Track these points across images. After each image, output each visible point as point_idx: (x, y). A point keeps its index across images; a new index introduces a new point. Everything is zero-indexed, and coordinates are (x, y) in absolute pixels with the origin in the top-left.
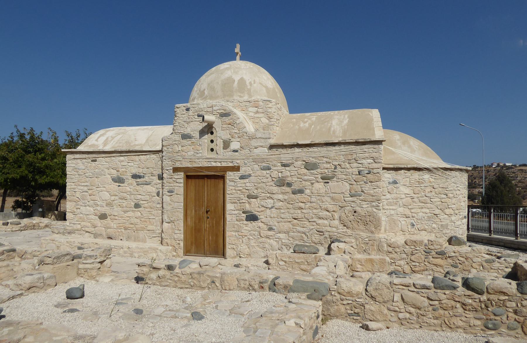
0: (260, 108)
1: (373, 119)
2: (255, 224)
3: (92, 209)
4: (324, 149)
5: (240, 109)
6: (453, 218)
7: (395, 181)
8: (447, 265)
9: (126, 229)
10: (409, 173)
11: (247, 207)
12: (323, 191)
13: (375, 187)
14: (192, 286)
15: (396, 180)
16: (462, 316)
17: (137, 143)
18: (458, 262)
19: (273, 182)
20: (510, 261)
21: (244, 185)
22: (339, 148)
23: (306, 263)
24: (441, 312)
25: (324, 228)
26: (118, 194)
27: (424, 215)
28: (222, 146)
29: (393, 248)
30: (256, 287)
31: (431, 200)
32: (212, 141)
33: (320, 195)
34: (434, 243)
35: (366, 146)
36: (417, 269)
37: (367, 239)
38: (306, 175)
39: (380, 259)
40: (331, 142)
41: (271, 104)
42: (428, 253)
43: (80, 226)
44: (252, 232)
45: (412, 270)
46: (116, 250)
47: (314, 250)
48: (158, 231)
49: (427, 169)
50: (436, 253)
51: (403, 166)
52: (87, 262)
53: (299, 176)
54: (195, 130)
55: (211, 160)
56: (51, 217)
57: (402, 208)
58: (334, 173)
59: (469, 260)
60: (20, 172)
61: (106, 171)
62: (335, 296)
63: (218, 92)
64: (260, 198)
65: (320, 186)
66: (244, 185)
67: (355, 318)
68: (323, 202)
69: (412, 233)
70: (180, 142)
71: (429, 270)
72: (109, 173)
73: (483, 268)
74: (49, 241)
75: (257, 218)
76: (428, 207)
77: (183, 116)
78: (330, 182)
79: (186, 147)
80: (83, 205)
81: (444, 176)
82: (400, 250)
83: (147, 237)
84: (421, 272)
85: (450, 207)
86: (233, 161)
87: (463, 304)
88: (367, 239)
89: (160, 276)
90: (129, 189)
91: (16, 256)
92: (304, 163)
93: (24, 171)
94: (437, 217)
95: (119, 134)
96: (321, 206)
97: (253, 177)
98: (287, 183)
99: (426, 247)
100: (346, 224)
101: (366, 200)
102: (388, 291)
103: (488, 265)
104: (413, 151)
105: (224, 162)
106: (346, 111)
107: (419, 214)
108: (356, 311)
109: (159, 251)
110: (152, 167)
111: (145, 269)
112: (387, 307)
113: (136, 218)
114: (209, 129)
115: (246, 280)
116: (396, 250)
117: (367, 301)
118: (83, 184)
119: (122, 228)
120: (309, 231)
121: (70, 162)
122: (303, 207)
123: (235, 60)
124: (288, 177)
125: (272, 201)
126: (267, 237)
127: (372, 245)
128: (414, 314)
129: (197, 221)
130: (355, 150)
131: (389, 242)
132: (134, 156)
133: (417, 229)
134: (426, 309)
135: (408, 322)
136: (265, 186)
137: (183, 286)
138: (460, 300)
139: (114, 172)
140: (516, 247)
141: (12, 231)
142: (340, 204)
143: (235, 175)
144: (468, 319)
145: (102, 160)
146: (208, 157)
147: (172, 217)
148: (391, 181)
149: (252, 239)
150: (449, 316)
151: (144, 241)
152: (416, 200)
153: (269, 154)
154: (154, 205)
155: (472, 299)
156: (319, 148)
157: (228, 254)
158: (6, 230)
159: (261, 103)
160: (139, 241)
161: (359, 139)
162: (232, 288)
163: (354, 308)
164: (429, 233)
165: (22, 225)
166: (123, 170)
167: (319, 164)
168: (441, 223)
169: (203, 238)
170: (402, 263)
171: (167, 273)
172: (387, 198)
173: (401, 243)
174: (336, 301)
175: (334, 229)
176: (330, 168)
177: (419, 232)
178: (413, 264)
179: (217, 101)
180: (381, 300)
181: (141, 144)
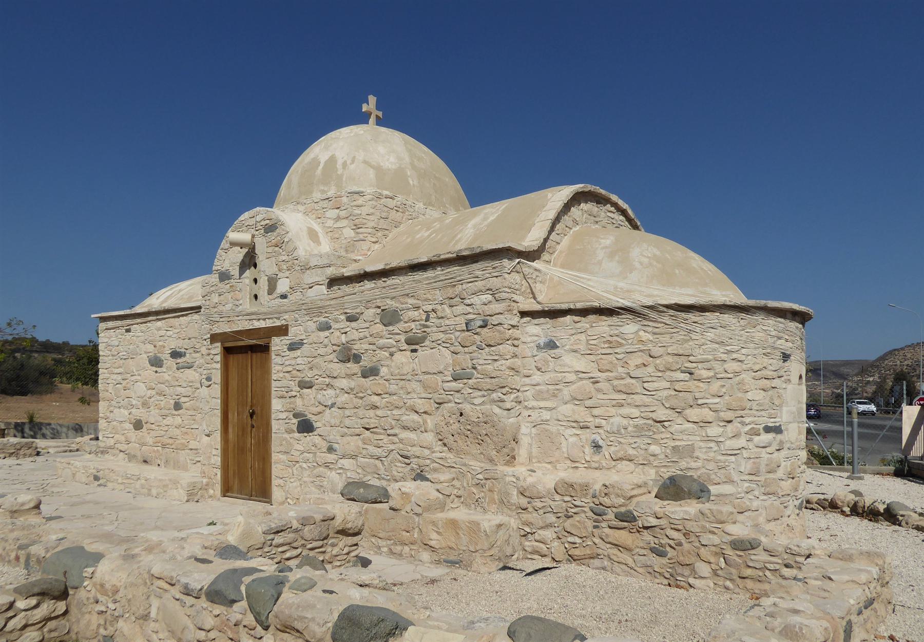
0: (343, 208)
3: (126, 412)
5: (314, 216)
6: (714, 431)
9: (164, 446)
10: (584, 323)
11: (299, 405)
13: (496, 358)
15: (553, 338)
18: (667, 541)
20: (796, 548)
25: (410, 448)
26: (154, 386)
27: (625, 422)
29: (529, 500)
31: (646, 385)
33: (404, 377)
37: (480, 476)
38: (381, 337)
39: (469, 523)
41: (362, 199)
42: (600, 515)
55: (254, 317)
58: (425, 329)
59: (693, 538)
65: (402, 358)
66: (293, 362)
69: (594, 465)
71: (602, 557)
75: (312, 426)
76: (637, 404)
81: (682, 325)
83: (189, 461)
84: (587, 560)
85: (700, 402)
88: (480, 476)
92: (379, 311)
96: (405, 401)
99: (594, 499)
100: (445, 441)
101: (480, 388)
105: (269, 319)
107: (612, 420)
116: (534, 504)
119: (160, 444)
120: (387, 454)
124: (355, 342)
126: (327, 465)
127: (490, 491)
130: (460, 275)
131: (521, 483)
139: (150, 348)
148: (542, 341)
153: (332, 296)
156: (401, 278)
164: (641, 466)
168: (673, 444)
170: (548, 534)
172: (534, 382)
177: (614, 463)
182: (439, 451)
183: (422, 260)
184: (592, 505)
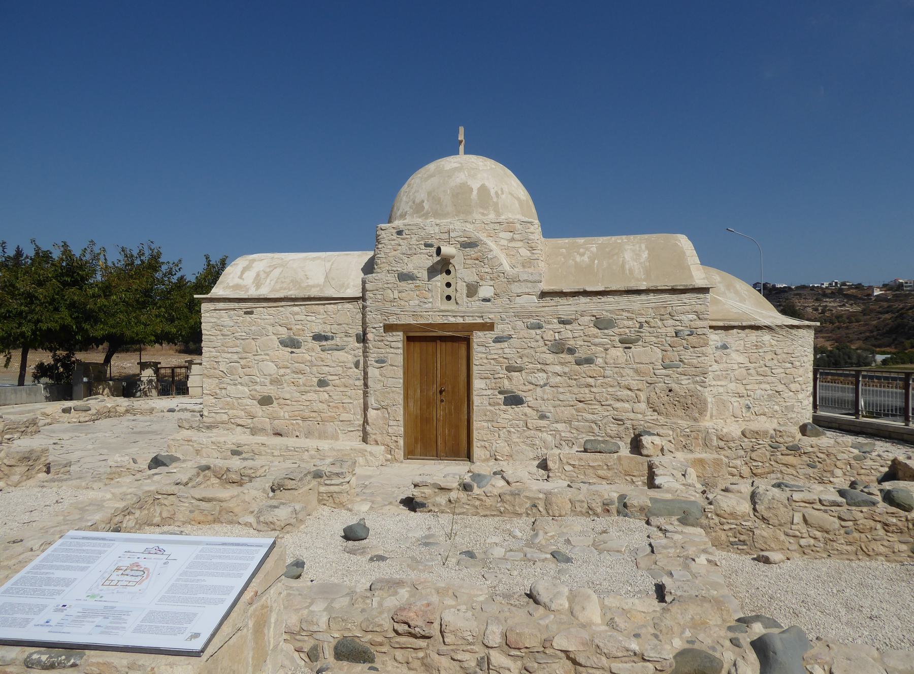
0: (516, 232)
1: (685, 253)
2: (518, 409)
3: (246, 389)
4: (624, 299)
7: (724, 344)
8: (802, 464)
9: (304, 419)
10: (743, 334)
11: (507, 384)
12: (622, 360)
13: (700, 355)
14: (501, 512)
16: (883, 539)
17: (311, 282)
18: (816, 459)
19: (547, 347)
21: (500, 352)
22: (646, 298)
23: (605, 467)
24: (856, 535)
25: (624, 414)
27: (763, 392)
28: (465, 292)
30: (599, 510)
31: (773, 370)
32: (448, 285)
33: (618, 366)
34: (784, 433)
35: (687, 295)
36: (759, 471)
37: (687, 430)
38: (597, 337)
40: (635, 288)
41: (532, 227)
43: (226, 416)
44: (514, 422)
45: (753, 473)
46: (296, 453)
47: (613, 449)
48: (357, 422)
49: (769, 328)
50: (787, 448)
51: (736, 324)
52: (333, 482)
53: (586, 338)
54: (420, 267)
56: (103, 392)
57: (734, 384)
58: (639, 334)
59: (832, 457)
60: (59, 318)
61: (269, 329)
62: (713, 519)
63: (446, 206)
64: (526, 371)
65: (617, 353)
66: (500, 352)
67: (740, 547)
68: (622, 376)
69: (746, 419)
70: (395, 286)
72: (274, 332)
73: (850, 468)
74: (182, 442)
75: (523, 400)
77: (393, 242)
78: (633, 347)
79: (407, 292)
80: (232, 382)
82: (735, 445)
86: (483, 314)
87: (885, 525)
88: (687, 430)
89: (452, 499)
90: (309, 358)
91: (212, 476)
93: (65, 316)
94: (780, 394)
95: (275, 268)
96: (620, 382)
97: (514, 339)
98: (569, 348)
100: (657, 408)
102: (785, 509)
103: (857, 463)
104: (742, 300)
106: (639, 236)
108: (742, 538)
109: (369, 455)
110: (346, 322)
111: (428, 491)
112: (784, 532)
113: (321, 402)
114: (443, 266)
115: (583, 502)
116: (729, 445)
117: (757, 526)
118: (230, 350)
119: (299, 418)
121: (208, 315)
122: (593, 384)
123: (458, 153)
125: (545, 375)
126: (538, 429)
128: (821, 539)
129: (425, 407)
131: (720, 433)
132: (317, 306)
133: (754, 413)
134: (837, 533)
135: (812, 551)
136: (533, 353)
137: (488, 513)
138: (882, 520)
140: (858, 429)
141: (79, 422)
142: (649, 379)
143: (487, 336)
144: (892, 543)
145: (263, 313)
146: (442, 308)
147: (384, 400)
148: (719, 344)
149: (515, 433)
150: (867, 540)
151: (335, 437)
152: (752, 371)
153: (541, 305)
154: (351, 382)
155: (896, 517)
156: (616, 297)
157: (476, 456)
158: (69, 420)
159: (518, 226)
160: (326, 438)
161: (677, 286)
162: (563, 513)
163: (738, 534)
165: (93, 411)
166: (298, 327)
167: (617, 321)
168: (785, 404)
169: (435, 433)
170: (738, 462)
171: (463, 495)
172: (714, 370)
173: (736, 434)
174: (714, 526)
175: (640, 416)
176: (633, 326)
178: (754, 464)
179: (449, 220)
180: (777, 522)
181: (318, 285)
182: (651, 416)
183: (641, 288)
184: (771, 443)
